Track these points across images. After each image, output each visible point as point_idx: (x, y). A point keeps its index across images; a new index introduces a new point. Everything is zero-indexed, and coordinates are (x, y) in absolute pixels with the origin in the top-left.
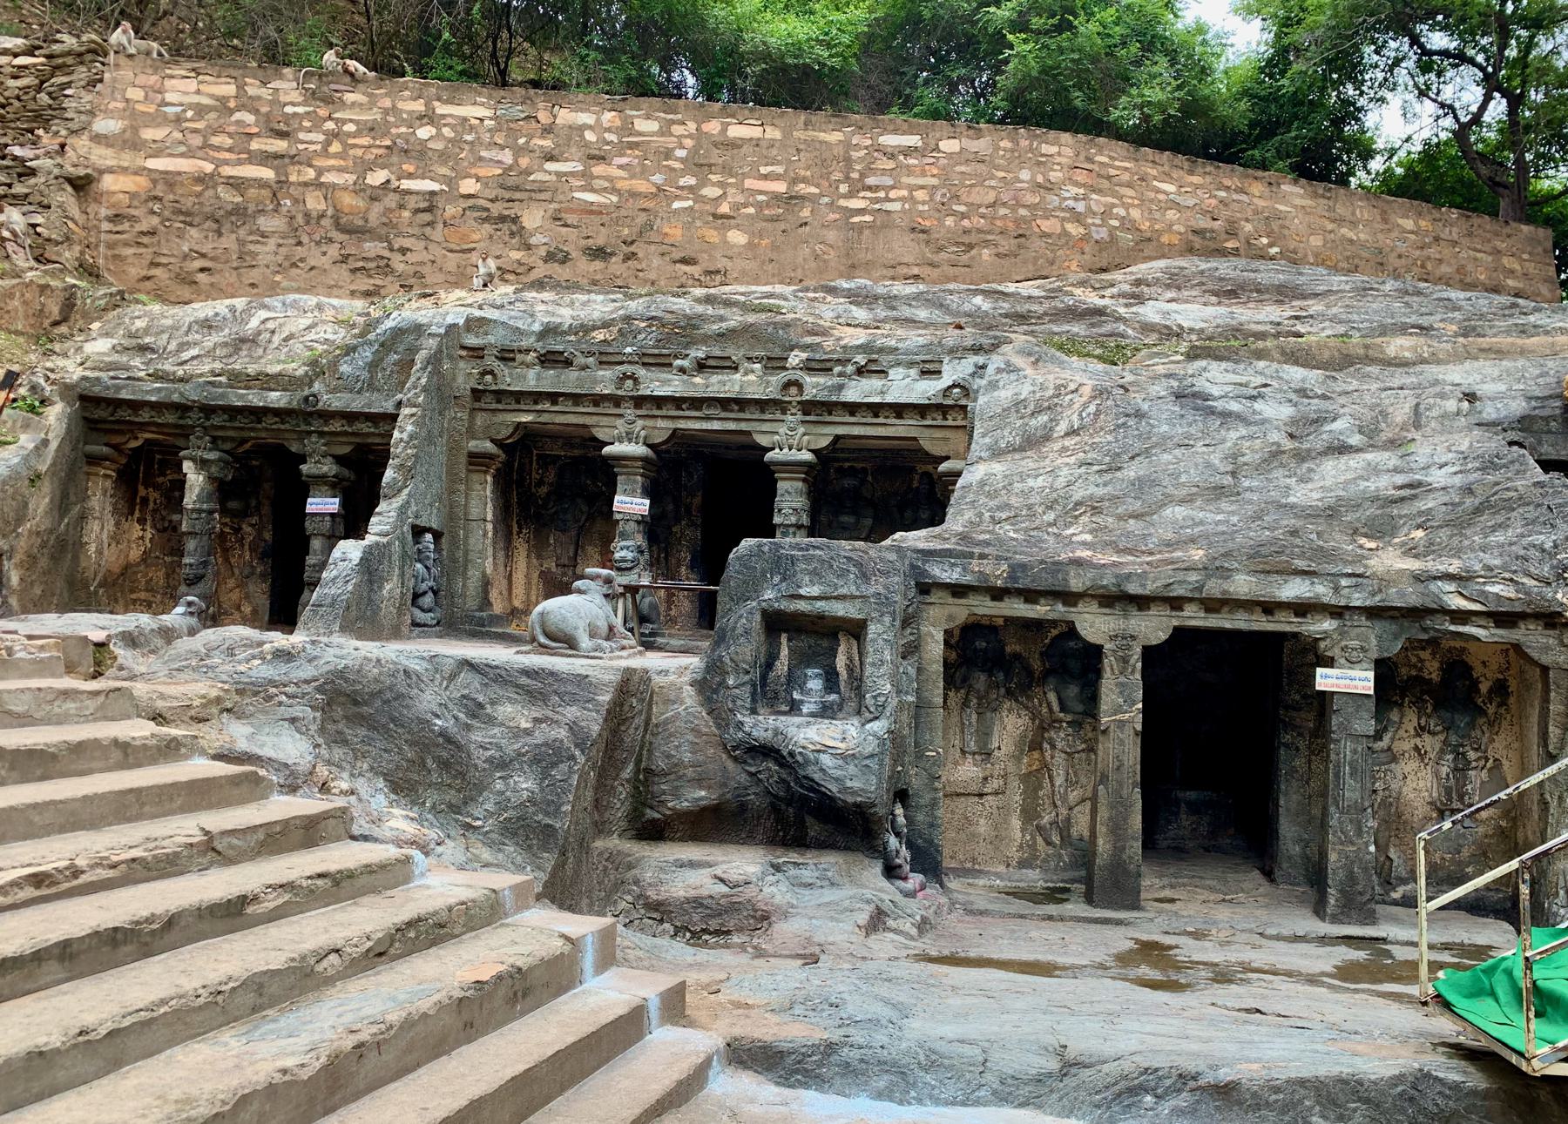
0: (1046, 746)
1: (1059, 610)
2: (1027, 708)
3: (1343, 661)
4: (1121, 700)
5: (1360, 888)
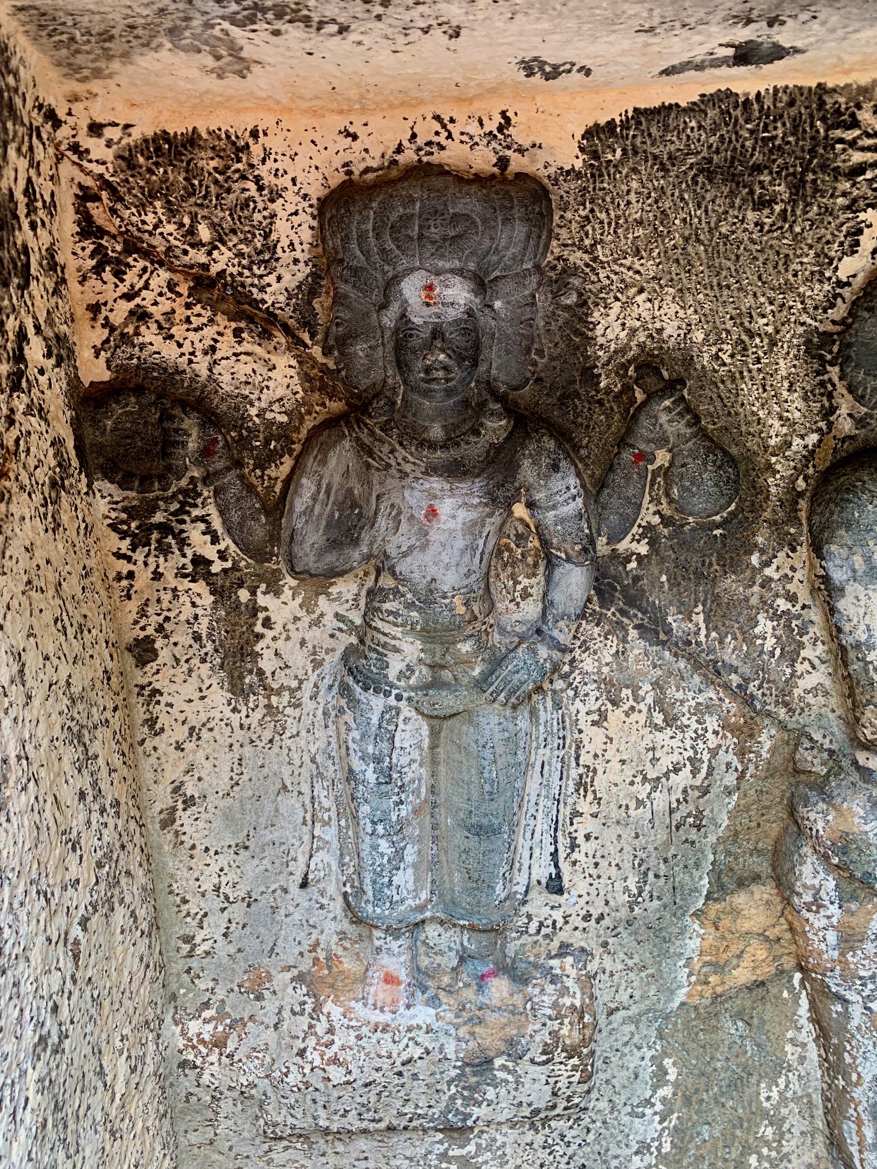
2: (713, 671)
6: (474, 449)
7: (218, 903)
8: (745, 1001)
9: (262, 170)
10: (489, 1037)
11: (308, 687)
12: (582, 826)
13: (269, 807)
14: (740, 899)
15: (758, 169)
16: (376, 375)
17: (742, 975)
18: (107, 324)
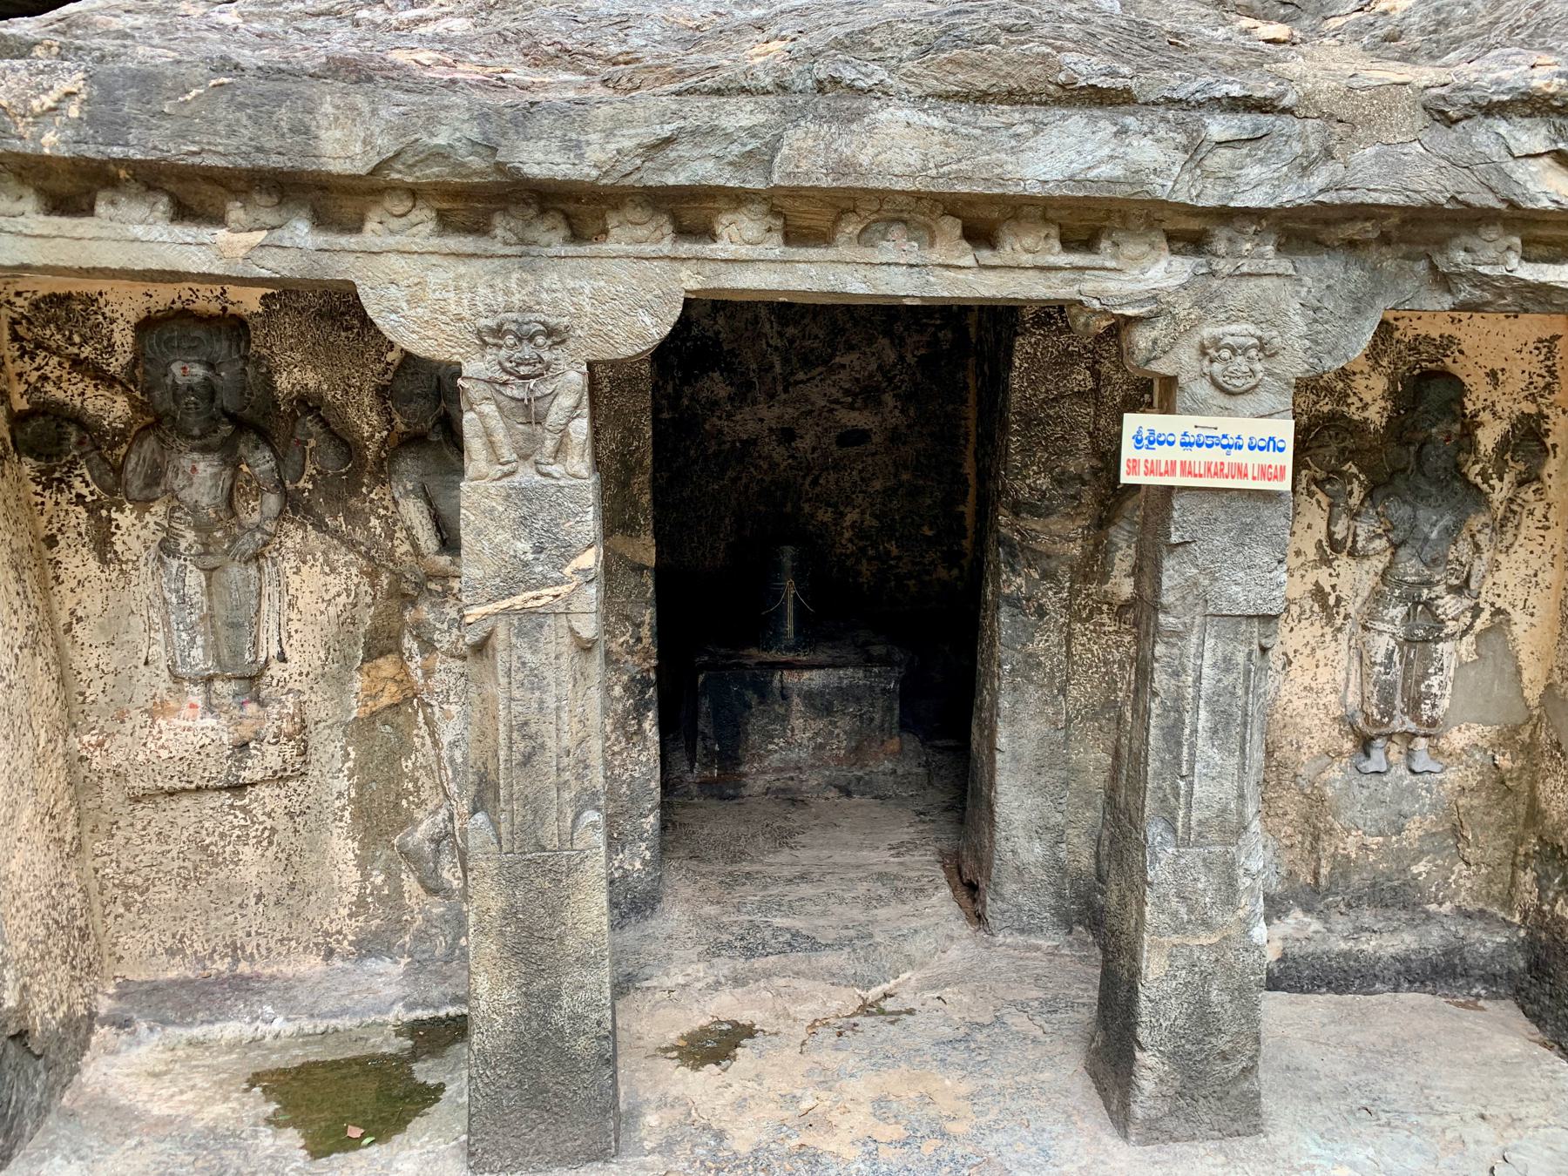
0: (409, 643)
1: (296, 247)
2: (352, 545)
3: (1203, 389)
4: (524, 546)
5: (1222, 1043)
6: (215, 439)
7: (98, 674)
8: (389, 715)
9: (106, 310)
10: (246, 732)
11: (142, 560)
12: (294, 626)
13: (125, 623)
14: (380, 661)
15: (343, 314)
16: (166, 406)
17: (385, 700)
18: (27, 382)
